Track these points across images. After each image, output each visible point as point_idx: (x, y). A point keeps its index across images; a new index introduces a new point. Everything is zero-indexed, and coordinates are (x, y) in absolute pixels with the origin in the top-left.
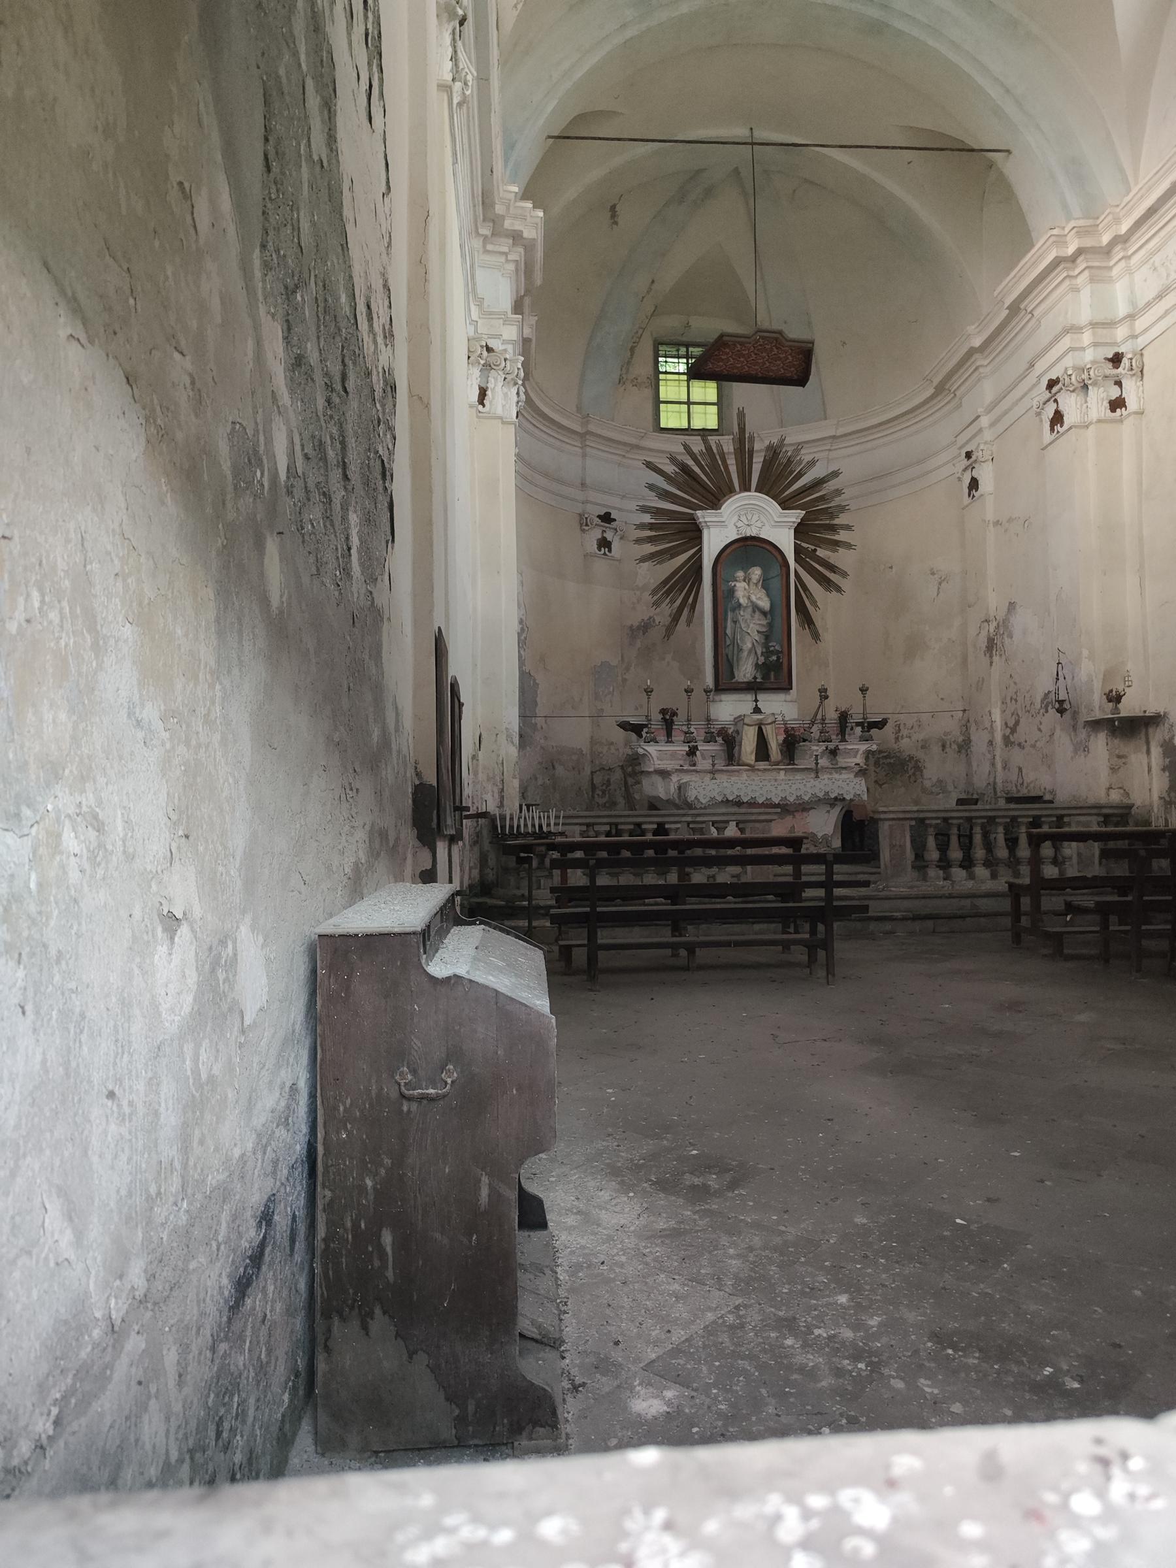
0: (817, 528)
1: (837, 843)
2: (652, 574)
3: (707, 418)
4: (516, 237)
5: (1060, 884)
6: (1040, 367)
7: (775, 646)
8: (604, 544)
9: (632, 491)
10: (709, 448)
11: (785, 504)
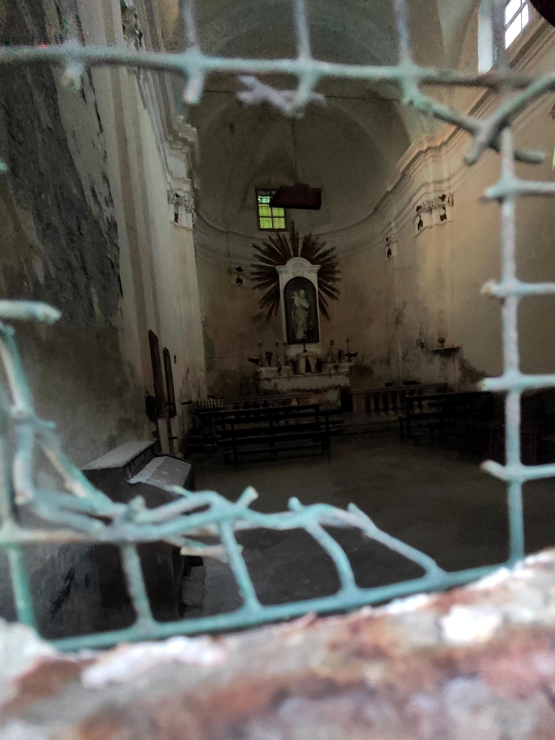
0: (326, 273)
1: (339, 403)
2: (259, 294)
3: (280, 224)
4: (185, 141)
5: (423, 416)
6: (414, 200)
7: (311, 323)
8: (239, 281)
9: (248, 257)
10: (279, 238)
11: (313, 262)
